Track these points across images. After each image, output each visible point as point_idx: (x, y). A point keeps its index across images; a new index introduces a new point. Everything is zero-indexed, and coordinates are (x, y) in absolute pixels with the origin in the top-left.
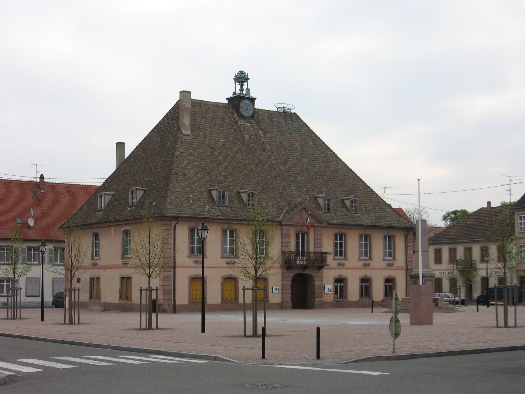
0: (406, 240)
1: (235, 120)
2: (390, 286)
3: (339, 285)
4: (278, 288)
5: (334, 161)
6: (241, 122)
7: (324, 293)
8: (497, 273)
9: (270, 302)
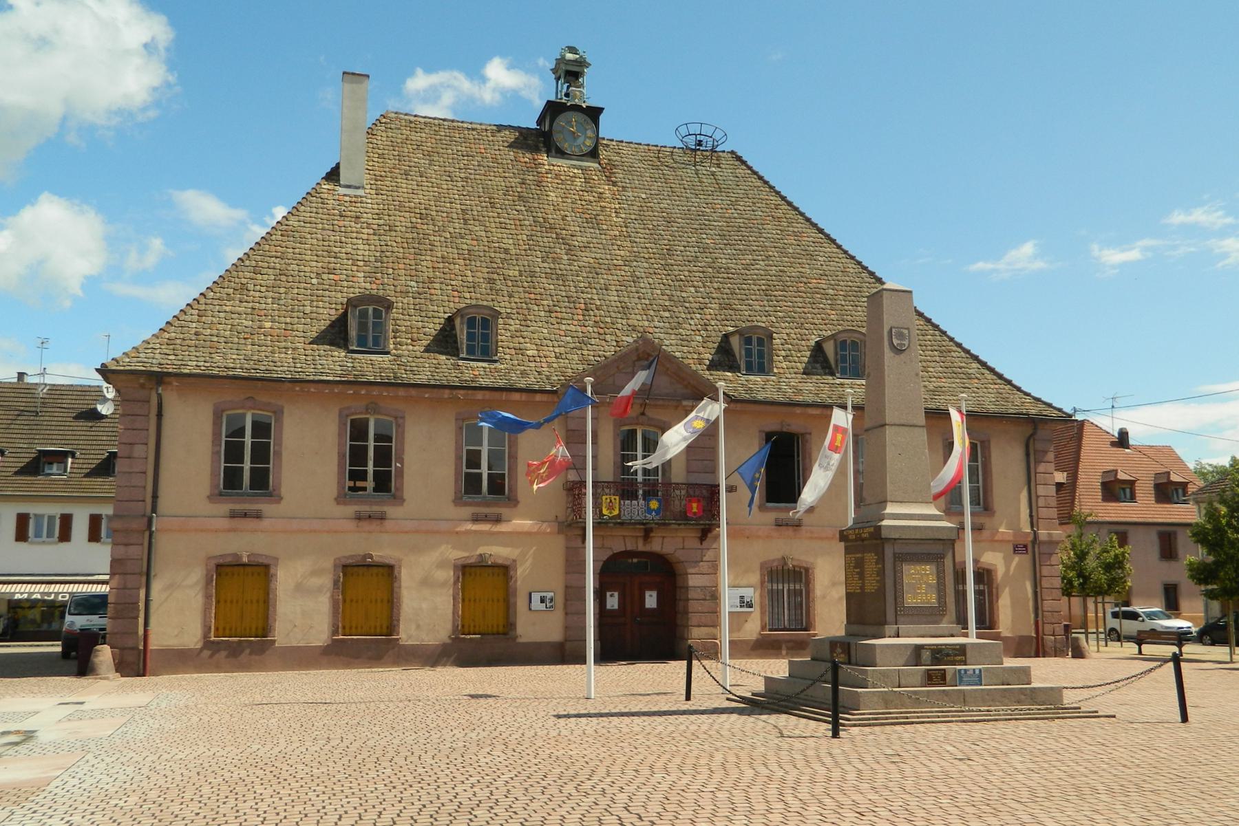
0: (1028, 455)
4: (550, 595)
9: (520, 640)
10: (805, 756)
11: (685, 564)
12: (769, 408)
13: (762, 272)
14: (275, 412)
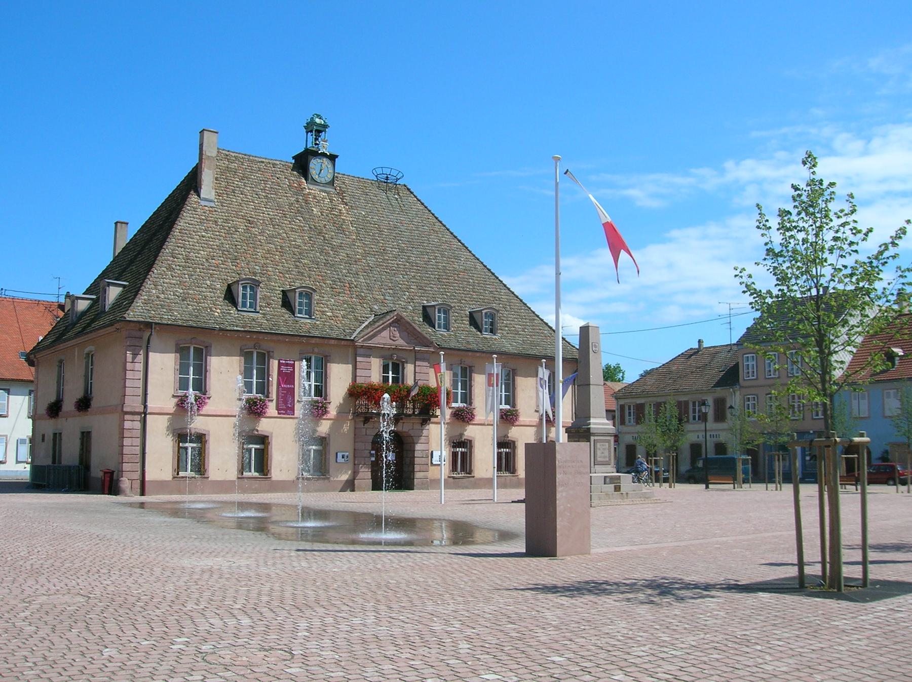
1: (300, 185)
2: (506, 453)
3: (459, 450)
4: (347, 454)
5: (462, 256)
6: (309, 189)
7: (432, 463)
8: (710, 435)
10: (307, 559)
11: (414, 438)
12: (456, 352)
13: (435, 267)
14: (206, 347)
